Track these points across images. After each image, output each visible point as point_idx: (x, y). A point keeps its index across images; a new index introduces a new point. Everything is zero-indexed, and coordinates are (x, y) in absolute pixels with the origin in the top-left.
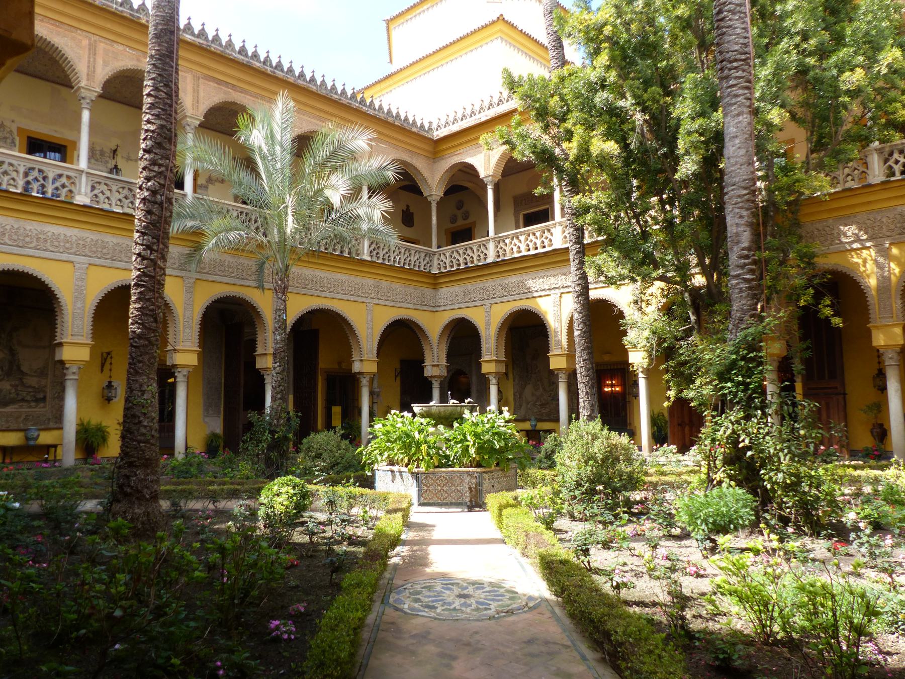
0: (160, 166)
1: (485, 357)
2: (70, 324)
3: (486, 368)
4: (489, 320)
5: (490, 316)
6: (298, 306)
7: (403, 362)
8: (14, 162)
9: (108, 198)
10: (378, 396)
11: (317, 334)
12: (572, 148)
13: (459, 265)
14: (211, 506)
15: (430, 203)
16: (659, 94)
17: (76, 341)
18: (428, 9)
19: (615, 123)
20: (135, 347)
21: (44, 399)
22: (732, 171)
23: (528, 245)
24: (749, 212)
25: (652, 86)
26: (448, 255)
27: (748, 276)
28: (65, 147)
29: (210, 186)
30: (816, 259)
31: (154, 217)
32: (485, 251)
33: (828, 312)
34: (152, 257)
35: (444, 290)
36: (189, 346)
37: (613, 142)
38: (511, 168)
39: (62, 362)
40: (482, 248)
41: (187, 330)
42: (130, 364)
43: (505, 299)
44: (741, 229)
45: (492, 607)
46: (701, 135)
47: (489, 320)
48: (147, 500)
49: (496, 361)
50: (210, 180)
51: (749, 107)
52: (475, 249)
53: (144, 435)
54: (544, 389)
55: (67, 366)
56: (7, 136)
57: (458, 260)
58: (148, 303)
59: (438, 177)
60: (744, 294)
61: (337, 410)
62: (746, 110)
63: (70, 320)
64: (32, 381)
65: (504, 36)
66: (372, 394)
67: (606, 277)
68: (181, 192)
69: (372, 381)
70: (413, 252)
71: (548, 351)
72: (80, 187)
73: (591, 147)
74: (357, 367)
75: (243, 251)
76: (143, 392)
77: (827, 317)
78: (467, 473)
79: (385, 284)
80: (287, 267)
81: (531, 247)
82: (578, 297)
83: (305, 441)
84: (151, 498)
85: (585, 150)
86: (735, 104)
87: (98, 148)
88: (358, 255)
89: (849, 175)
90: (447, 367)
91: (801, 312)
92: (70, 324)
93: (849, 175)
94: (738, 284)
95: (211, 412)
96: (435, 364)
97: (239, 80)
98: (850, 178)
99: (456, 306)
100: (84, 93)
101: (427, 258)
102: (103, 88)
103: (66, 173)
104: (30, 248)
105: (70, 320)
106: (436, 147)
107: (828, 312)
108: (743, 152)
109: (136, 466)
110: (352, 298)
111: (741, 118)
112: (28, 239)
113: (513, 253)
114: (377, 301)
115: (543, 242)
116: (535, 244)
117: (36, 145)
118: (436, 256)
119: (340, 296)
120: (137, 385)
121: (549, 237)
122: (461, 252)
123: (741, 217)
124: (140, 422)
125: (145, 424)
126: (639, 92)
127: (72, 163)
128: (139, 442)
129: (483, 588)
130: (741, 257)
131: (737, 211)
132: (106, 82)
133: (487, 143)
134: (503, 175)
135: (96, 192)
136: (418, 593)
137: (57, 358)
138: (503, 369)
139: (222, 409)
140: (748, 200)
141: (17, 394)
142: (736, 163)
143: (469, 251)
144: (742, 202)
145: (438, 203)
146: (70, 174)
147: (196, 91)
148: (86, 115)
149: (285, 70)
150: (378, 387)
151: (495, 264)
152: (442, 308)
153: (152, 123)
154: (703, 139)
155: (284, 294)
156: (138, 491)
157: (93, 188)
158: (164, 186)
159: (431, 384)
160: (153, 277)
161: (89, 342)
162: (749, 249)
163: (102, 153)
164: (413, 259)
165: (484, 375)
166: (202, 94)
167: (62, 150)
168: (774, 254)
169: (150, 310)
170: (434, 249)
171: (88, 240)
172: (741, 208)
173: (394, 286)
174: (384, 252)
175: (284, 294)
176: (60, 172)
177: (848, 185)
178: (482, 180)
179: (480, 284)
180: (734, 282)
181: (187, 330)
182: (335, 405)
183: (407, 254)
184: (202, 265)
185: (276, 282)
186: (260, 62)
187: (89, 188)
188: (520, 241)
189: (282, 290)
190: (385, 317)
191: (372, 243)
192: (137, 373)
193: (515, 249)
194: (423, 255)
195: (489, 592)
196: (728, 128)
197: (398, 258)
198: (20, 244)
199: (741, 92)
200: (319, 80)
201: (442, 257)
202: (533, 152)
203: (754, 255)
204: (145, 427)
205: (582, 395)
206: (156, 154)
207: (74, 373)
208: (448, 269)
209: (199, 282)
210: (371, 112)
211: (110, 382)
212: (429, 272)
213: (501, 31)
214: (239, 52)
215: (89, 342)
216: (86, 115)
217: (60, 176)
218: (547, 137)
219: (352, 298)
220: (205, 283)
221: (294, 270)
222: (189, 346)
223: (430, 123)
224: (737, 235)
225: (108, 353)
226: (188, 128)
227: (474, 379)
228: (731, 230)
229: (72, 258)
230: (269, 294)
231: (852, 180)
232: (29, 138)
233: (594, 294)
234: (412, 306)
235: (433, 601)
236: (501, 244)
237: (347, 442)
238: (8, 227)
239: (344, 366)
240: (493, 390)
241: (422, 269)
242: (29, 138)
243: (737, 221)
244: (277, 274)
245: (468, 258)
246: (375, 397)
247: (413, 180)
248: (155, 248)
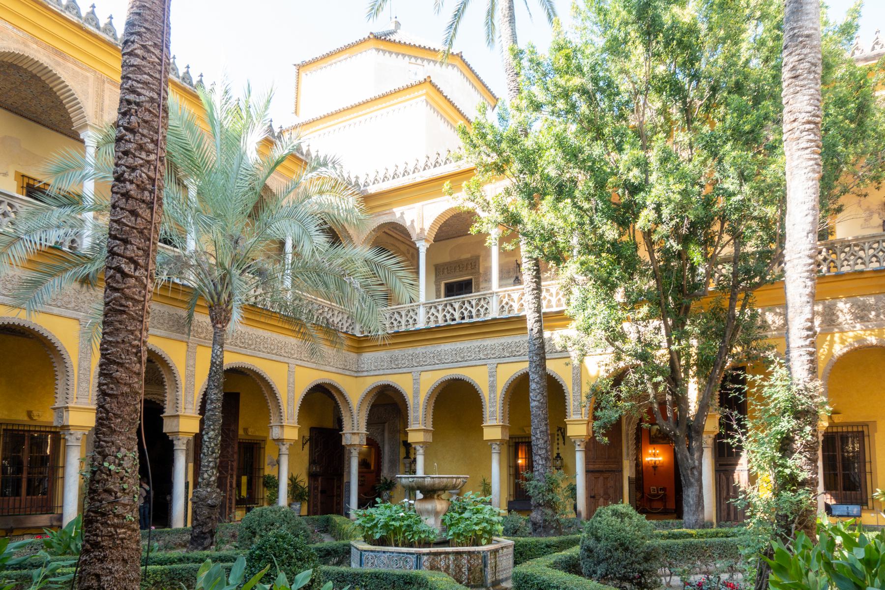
1: (488, 421)
7: (312, 429)
23: (462, 313)
32: (414, 317)
34: (137, 274)
36: (87, 404)
40: (411, 313)
43: (437, 367)
65: (429, 100)
70: (336, 312)
71: (482, 421)
82: (536, 367)
99: (381, 372)
101: (350, 321)
110: (274, 357)
116: (470, 312)
119: (261, 355)
138: (430, 438)
145: (428, 250)
151: (429, 331)
152: (365, 374)
169: (133, 346)
181: (84, 385)
186: (178, 77)
190: (307, 377)
207: (77, 439)
222: (87, 404)
223: (357, 177)
231: (862, 263)
234: (334, 370)
236: (433, 310)
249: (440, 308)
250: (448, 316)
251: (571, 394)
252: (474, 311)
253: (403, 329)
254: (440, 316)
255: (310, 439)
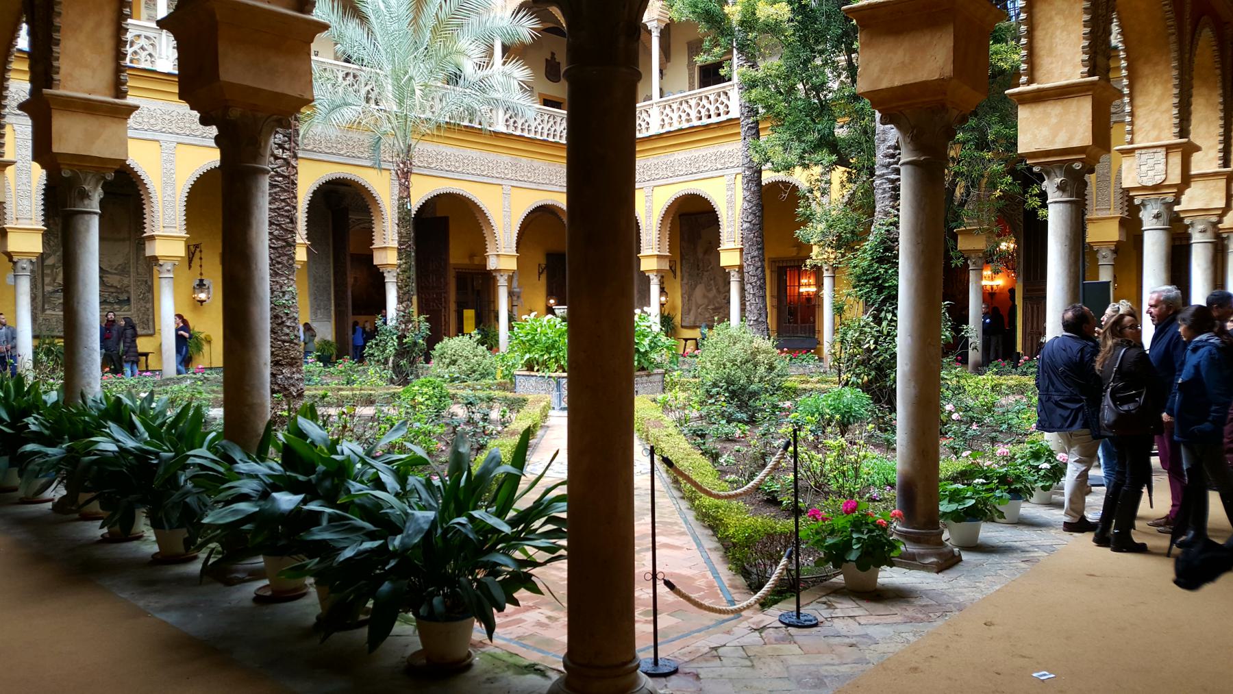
1: (645, 251)
2: (161, 214)
6: (422, 191)
21: (129, 299)
32: (647, 119)
43: (670, 181)
49: (659, 257)
53: (287, 334)
55: (161, 262)
61: (469, 314)
66: (511, 294)
69: (510, 279)
71: (718, 243)
73: (757, 12)
74: (492, 264)
76: (284, 293)
83: (438, 346)
92: (161, 214)
95: (320, 316)
103: (144, 33)
114: (515, 183)
115: (718, 108)
121: (726, 101)
127: (139, 19)
128: (284, 341)
130: (886, 156)
137: (148, 253)
139: (333, 313)
146: (148, 34)
150: (519, 287)
151: (659, 137)
160: (288, 177)
161: (183, 234)
168: (968, 135)
171: (174, 114)
173: (536, 163)
175: (407, 179)
176: (138, 33)
182: (467, 308)
183: (552, 122)
189: (405, 176)
205: (749, 297)
211: (201, 281)
225: (196, 246)
229: (158, 136)
237: (484, 348)
249: (693, 102)
250: (704, 112)
251: (160, 205)
252: (712, 108)
253: (676, 126)
254: (675, 116)
255: (547, 267)
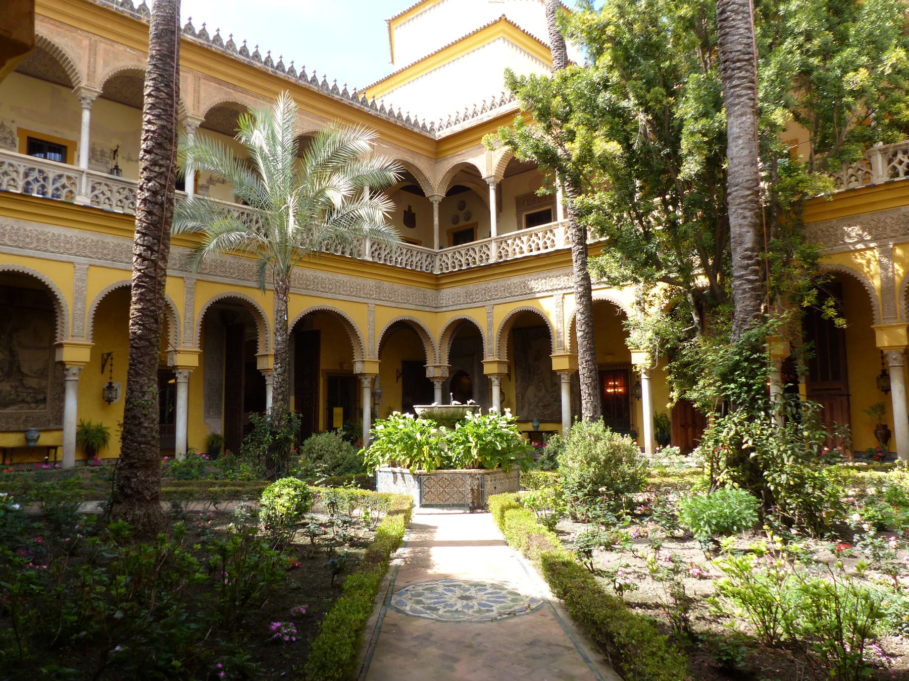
0: (161, 166)
1: (488, 358)
2: (70, 325)
3: (488, 369)
4: (491, 321)
5: (492, 317)
6: (299, 307)
7: (404, 363)
8: (15, 163)
9: (108, 199)
10: (380, 397)
11: (318, 335)
12: (574, 148)
13: (461, 266)
14: (212, 508)
15: (432, 204)
16: (662, 94)
17: (76, 342)
18: (430, 9)
19: (618, 124)
20: (135, 348)
21: (44, 400)
22: (735, 172)
23: (530, 246)
24: (752, 213)
25: (655, 87)
26: (450, 256)
27: (751, 277)
28: (65, 147)
29: (211, 187)
30: (819, 260)
31: (154, 218)
32: (487, 252)
33: (832, 312)
34: (153, 258)
35: (446, 290)
36: (190, 347)
37: (615, 143)
38: (513, 169)
39: (62, 364)
40: (484, 249)
41: (188, 331)
42: (130, 365)
43: (508, 300)
44: (744, 230)
45: (494, 608)
46: (704, 135)
47: (491, 321)
48: (148, 501)
49: (498, 362)
50: (211, 181)
51: (753, 107)
52: (477, 249)
53: (145, 436)
54: (547, 390)
55: (67, 367)
56: (7, 136)
57: (460, 261)
58: (149, 304)
59: (440, 177)
60: (748, 295)
61: (338, 411)
62: (749, 110)
63: (71, 321)
64: (33, 382)
65: (506, 36)
66: (373, 395)
67: (609, 277)
68: (182, 192)
69: (373, 382)
70: (415, 253)
71: (550, 352)
72: (81, 188)
73: (594, 148)
74: (358, 368)
75: (244, 251)
76: (144, 394)
77: (831, 318)
78: (469, 474)
79: (386, 285)
80: (289, 267)
81: (533, 247)
82: (580, 298)
83: (306, 442)
84: (152, 499)
85: (587, 150)
86: (738, 104)
87: (99, 149)
88: (360, 256)
89: (852, 175)
90: (449, 368)
91: (804, 313)
92: (70, 325)
93: (852, 175)
94: (741, 285)
95: (212, 413)
96: (437, 365)
97: (240, 80)
98: (853, 178)
99: (458, 307)
100: (84, 93)
101: (429, 259)
102: (104, 88)
103: (66, 173)
104: (30, 249)
105: (71, 321)
106: (438, 147)
107: (832, 312)
108: (746, 152)
109: (137, 468)
110: (354, 299)
111: (744, 118)
112: (28, 240)
113: (515, 254)
114: (378, 302)
115: (545, 243)
116: (538, 244)
117: (36, 146)
118: (438, 257)
119: (341, 297)
120: (138, 386)
121: (552, 237)
122: (463, 252)
123: (744, 217)
124: (141, 423)
125: (146, 425)
126: (642, 93)
127: (72, 164)
128: (140, 443)
129: (486, 590)
130: (745, 258)
131: (740, 211)
132: (106, 83)
133: (489, 144)
134: (505, 176)
135: (96, 192)
136: (420, 595)
137: (57, 359)
138: (505, 370)
139: (223, 410)
140: (751, 201)
141: (18, 396)
142: (740, 164)
143: (471, 252)
144: (745, 202)
145: (440, 204)
146: (71, 174)
147: (197, 91)
148: (86, 116)
149: (287, 70)
150: (380, 388)
151: (497, 265)
152: (444, 309)
153: (153, 124)
154: (706, 139)
155: (285, 295)
156: (139, 493)
157: (93, 189)
158: (165, 186)
159: (432, 385)
160: (154, 278)
161: (90, 343)
162: (752, 250)
163: (103, 153)
164: (415, 260)
165: (486, 376)
166: (202, 94)
167: (62, 150)
168: (778, 255)
169: (151, 311)
170: (436, 250)
171: (89, 241)
172: (745, 208)
173: (396, 286)
174: (386, 252)
175: (285, 295)
176: (60, 172)
177: (851, 186)
178: (484, 181)
179: (482, 285)
180: (737, 283)
181: (188, 331)
182: (337, 406)
183: (409, 254)
184: (203, 266)
185: (278, 283)
186: (261, 62)
187: (90, 189)
188: (523, 242)
189: (284, 291)
190: (387, 318)
191: (373, 244)
192: (138, 374)
193: (517, 250)
194: (425, 256)
195: (491, 593)
196: (731, 128)
197: (399, 259)
198: (21, 245)
199: (744, 92)
200: (320, 81)
201: (444, 258)
202: (535, 153)
203: (757, 256)
204: (146, 428)
205: (584, 396)
206: (156, 154)
207: (74, 374)
208: (450, 270)
209: (199, 283)
210: (372, 112)
211: (110, 384)
212: (431, 273)
213: (503, 31)
214: (241, 53)
215: (90, 343)
216: (86, 116)
217: (60, 176)
218: (549, 137)
219: (354, 299)
220: (206, 284)
221: (296, 271)
222: (190, 347)
223: (432, 123)
224: (741, 235)
225: (109, 355)
226: (188, 128)
227: (476, 381)
228: (735, 230)
229: (73, 258)
230: (270, 295)
231: (856, 180)
232: (29, 138)
233: (596, 295)
234: (413, 307)
235: (435, 603)
236: (504, 245)
237: (349, 443)
238: (8, 228)
239: (345, 367)
240: (496, 391)
241: (424, 269)
242: (29, 138)
243: (740, 221)
244: (278, 274)
245: (470, 259)
246: (377, 398)
247: (415, 181)
248: (156, 248)
